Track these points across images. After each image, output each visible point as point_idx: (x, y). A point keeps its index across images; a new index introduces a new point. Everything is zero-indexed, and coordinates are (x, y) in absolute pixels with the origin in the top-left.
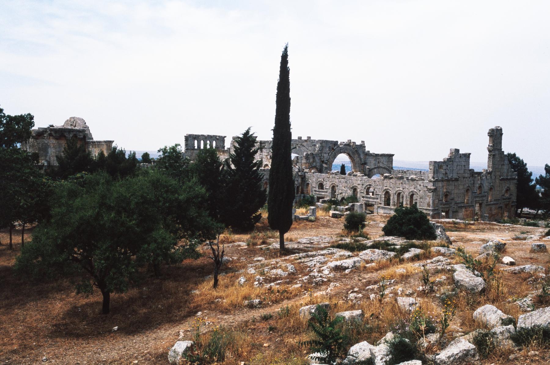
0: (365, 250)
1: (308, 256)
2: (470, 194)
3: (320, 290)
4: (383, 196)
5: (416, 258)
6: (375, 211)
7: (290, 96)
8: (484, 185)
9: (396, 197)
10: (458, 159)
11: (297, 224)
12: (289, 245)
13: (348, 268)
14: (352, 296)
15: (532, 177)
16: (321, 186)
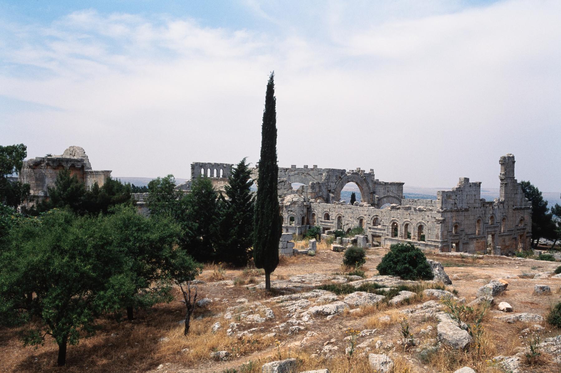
0: (351, 292)
1: (292, 299)
2: (481, 224)
3: (295, 340)
4: (391, 227)
5: (407, 302)
6: (382, 243)
7: (277, 127)
8: (497, 215)
9: (403, 228)
10: (469, 188)
11: (295, 258)
12: (277, 284)
13: (330, 314)
14: (326, 348)
15: (548, 207)
16: (327, 217)
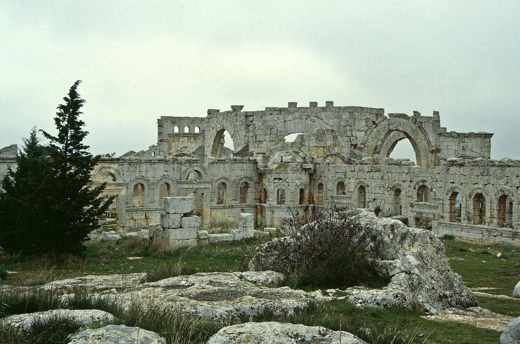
16: (341, 185)
